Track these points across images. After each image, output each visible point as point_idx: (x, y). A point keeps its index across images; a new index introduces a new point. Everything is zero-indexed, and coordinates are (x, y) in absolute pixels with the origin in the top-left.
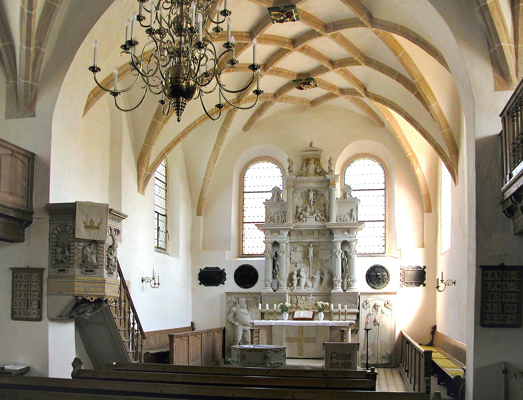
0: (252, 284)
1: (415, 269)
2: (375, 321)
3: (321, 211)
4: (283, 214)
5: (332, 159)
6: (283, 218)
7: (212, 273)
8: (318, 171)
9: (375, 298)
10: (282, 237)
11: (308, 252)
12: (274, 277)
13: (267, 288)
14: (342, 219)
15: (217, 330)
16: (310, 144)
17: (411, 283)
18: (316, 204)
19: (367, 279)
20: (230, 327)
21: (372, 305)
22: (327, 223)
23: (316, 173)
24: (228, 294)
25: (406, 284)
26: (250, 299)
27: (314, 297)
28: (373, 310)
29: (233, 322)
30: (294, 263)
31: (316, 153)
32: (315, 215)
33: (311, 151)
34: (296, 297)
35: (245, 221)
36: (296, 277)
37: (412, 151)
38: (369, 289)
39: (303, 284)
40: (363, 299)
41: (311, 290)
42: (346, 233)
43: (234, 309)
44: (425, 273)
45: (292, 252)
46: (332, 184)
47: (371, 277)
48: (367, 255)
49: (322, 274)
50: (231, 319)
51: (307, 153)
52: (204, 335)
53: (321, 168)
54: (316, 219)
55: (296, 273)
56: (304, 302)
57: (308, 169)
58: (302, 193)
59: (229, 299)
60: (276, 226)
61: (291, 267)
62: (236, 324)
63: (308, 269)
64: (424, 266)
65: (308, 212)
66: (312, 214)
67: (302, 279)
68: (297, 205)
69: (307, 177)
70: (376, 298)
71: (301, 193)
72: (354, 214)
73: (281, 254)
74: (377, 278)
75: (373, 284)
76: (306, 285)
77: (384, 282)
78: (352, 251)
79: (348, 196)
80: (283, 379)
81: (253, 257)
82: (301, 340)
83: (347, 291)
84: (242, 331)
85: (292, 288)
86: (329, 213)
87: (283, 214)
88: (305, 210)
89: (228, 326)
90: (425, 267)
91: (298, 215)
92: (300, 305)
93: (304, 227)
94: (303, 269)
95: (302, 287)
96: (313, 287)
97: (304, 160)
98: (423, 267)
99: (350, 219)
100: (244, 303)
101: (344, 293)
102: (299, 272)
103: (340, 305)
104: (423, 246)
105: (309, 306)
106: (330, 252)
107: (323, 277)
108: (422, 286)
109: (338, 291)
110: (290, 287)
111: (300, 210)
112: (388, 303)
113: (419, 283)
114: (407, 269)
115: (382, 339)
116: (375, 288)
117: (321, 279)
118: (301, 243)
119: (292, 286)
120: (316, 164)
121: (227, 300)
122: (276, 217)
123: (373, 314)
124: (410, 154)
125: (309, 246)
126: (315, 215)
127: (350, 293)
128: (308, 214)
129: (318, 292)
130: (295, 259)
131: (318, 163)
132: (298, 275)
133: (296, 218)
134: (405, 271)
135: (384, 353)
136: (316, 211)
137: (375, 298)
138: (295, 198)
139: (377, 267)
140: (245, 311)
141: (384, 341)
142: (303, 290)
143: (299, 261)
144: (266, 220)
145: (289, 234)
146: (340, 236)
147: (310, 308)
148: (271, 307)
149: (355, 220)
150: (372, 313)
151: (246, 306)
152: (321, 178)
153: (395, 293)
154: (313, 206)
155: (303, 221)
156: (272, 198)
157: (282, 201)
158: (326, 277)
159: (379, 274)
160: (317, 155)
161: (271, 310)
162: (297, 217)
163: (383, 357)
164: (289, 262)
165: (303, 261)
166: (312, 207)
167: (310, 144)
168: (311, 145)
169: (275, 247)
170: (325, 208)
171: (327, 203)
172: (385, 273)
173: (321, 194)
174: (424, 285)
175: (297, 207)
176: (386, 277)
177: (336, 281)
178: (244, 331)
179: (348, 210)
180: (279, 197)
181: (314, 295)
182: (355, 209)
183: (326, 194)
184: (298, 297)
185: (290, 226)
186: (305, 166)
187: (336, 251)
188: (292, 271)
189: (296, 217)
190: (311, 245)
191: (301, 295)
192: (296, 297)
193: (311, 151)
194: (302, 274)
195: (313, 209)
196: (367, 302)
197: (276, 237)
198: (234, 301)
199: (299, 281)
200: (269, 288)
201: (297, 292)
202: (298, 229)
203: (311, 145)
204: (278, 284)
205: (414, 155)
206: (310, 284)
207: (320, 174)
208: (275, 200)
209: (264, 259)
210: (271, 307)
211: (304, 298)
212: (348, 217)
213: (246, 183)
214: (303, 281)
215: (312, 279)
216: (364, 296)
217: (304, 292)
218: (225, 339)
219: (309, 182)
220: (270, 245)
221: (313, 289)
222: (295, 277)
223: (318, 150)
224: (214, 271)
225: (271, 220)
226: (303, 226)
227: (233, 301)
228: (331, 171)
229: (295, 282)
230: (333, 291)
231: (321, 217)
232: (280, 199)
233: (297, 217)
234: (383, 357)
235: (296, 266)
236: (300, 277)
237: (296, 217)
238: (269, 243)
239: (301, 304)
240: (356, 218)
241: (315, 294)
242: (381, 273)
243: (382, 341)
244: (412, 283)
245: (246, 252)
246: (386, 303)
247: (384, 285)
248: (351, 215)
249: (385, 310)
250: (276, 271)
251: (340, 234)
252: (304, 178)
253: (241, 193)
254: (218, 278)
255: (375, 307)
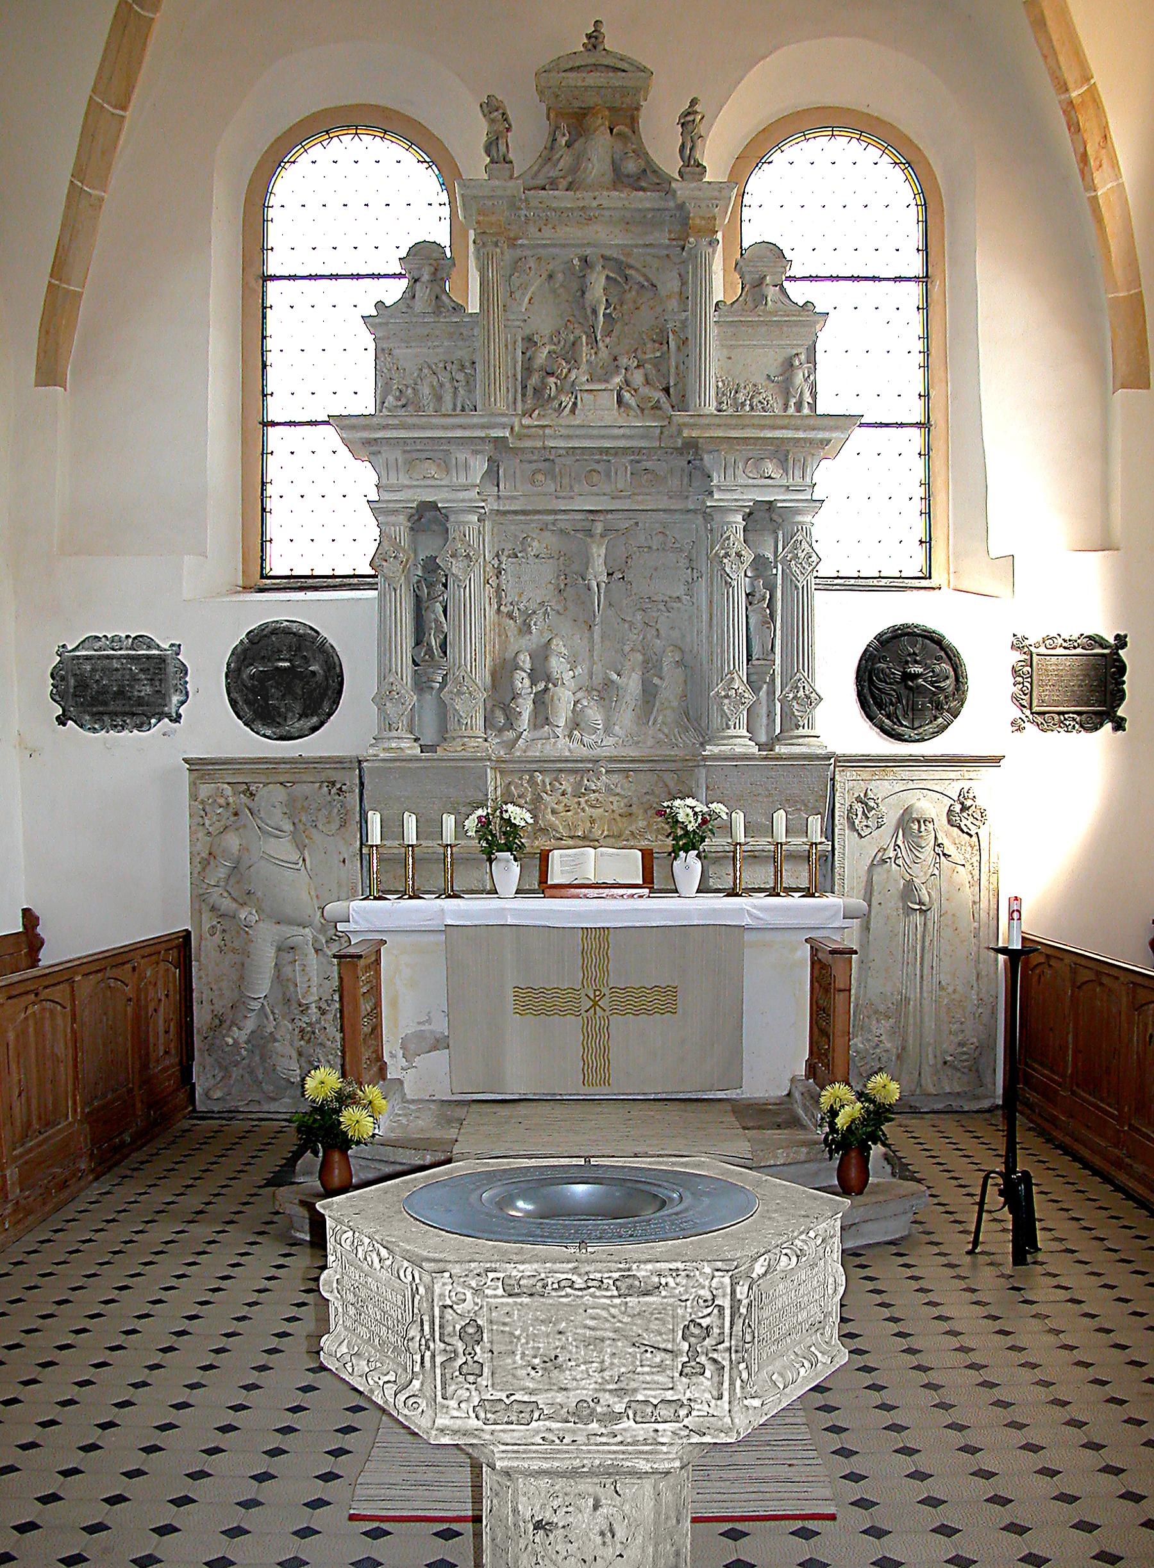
0: (315, 720)
1: (1079, 651)
2: (909, 890)
3: (646, 361)
4: (460, 376)
5: (698, 108)
6: (462, 392)
7: (116, 664)
8: (631, 167)
9: (899, 786)
10: (462, 480)
11: (587, 562)
12: (421, 685)
13: (394, 734)
14: (743, 404)
15: (151, 949)
16: (589, 37)
17: (1059, 713)
18: (618, 326)
19: (860, 694)
20: (213, 931)
21: (891, 819)
22: (680, 417)
23: (619, 179)
24: (199, 768)
25: (1040, 719)
26: (306, 789)
27: (615, 778)
28: (899, 842)
29: (226, 904)
30: (516, 613)
31: (616, 80)
32: (618, 380)
33: (595, 67)
34: (532, 781)
35: (271, 417)
36: (527, 682)
37: (1086, 78)
38: (877, 744)
39: (562, 719)
40: (848, 786)
41: (609, 746)
42: (770, 468)
43: (232, 841)
44: (1122, 669)
45: (503, 559)
46: (700, 232)
47: (881, 685)
48: (852, 582)
49: (651, 666)
50: (220, 890)
51: (573, 79)
52: (86, 987)
53: (640, 153)
54: (620, 401)
55: (525, 661)
56: (572, 802)
57: (579, 158)
58: (550, 277)
59: (205, 790)
60: (432, 427)
61: (502, 633)
62: (1135, 1165)
63: (579, 642)
64: (1117, 637)
65: (584, 367)
66: (600, 375)
67: (559, 690)
68: (528, 332)
69: (579, 195)
70: (911, 785)
71: (544, 276)
72: (799, 378)
73: (456, 567)
74: (910, 688)
75: (888, 717)
76: (575, 724)
77: (939, 707)
78: (802, 555)
79: (772, 292)
80: (202, 973)
81: (315, 588)
82: (595, 1004)
83: (780, 749)
84: (271, 952)
85: (510, 735)
86: (681, 377)
87: (460, 376)
88: (573, 360)
89: (206, 927)
90: (1121, 641)
91: (534, 380)
92: (550, 817)
93: (569, 437)
94: (558, 645)
95: (559, 731)
96: (608, 731)
97: (560, 115)
98: (1112, 641)
99: (781, 402)
100: (278, 812)
101: (766, 758)
102: (541, 655)
103: (780, 817)
104: (1105, 546)
105: (592, 822)
106: (683, 563)
107: (656, 680)
108: (1108, 726)
109: (738, 750)
110: (501, 730)
111: (542, 356)
112: (964, 808)
113: (1095, 713)
114: (1042, 650)
115: (942, 977)
116: (899, 737)
117: (649, 694)
118: (551, 518)
119: (510, 725)
120: (619, 134)
121: (194, 797)
122: (426, 390)
123: (899, 861)
124: (1077, 88)
125: (589, 533)
126: (618, 380)
127: (792, 757)
128: (580, 376)
129: (633, 753)
130: (520, 595)
131: (626, 130)
132: (540, 673)
133: (524, 395)
134: (1035, 658)
135: (949, 1045)
136: (624, 361)
137: (899, 786)
138: (517, 295)
139: (908, 634)
140: (283, 849)
141: (950, 990)
142: (563, 746)
143: (542, 604)
144: (381, 403)
145: (493, 474)
146: (741, 481)
147: (597, 833)
148: (429, 828)
149: (806, 411)
150: (892, 854)
151: (288, 827)
152: (645, 200)
153: (995, 761)
154: (607, 340)
155: (560, 408)
156: (410, 295)
157: (458, 308)
158: (670, 687)
159: (918, 669)
160: (624, 91)
161: (795, 840)
162: (530, 391)
163: (945, 1063)
164: (491, 612)
165: (559, 602)
166: (600, 344)
167: (589, 37)
168: (594, 39)
169: (422, 537)
170: (665, 347)
171: (670, 325)
172: (946, 667)
173: (641, 279)
174: (1119, 725)
175: (529, 340)
176: (949, 684)
177: (726, 701)
178: (286, 949)
179: (769, 360)
180: (438, 290)
181: (622, 766)
182: (803, 357)
183: (669, 284)
184: (539, 778)
185: (503, 426)
186: (568, 145)
187: (727, 555)
188: (509, 655)
189: (524, 387)
190: (599, 528)
191: (558, 767)
192: (532, 781)
193: (595, 67)
194: (557, 665)
195: (604, 353)
196: (871, 803)
197: (433, 483)
198: (231, 800)
199: (541, 702)
200: (400, 733)
201: (535, 753)
202: (539, 444)
203: (594, 39)
204: (443, 712)
205: (1093, 95)
206: (595, 715)
207: (636, 182)
208: (419, 305)
209: (373, 594)
210: (429, 828)
211: (567, 784)
212: (770, 395)
213: (275, 235)
214: (564, 699)
215: (605, 692)
216: (850, 774)
217: (567, 754)
218: (191, 991)
219: (587, 217)
220: (401, 527)
221: (610, 741)
222: (522, 681)
223: (625, 66)
224: (127, 657)
225: (403, 401)
226: (563, 431)
227: (222, 801)
228: (692, 167)
229: (526, 707)
230: (711, 750)
231: (645, 391)
232: (444, 298)
233: (530, 391)
234: (945, 1063)
235: (525, 629)
236: (548, 679)
237: (524, 387)
238: (395, 512)
239: (553, 812)
240: (808, 398)
241: (621, 761)
242: (926, 667)
243: (942, 988)
244: (1063, 713)
245: (278, 566)
246: (958, 807)
247: (940, 720)
248: (786, 388)
249: (950, 838)
250: (430, 650)
251: (739, 472)
252: (562, 198)
253: (253, 283)
254: (148, 689)
255: (908, 823)
